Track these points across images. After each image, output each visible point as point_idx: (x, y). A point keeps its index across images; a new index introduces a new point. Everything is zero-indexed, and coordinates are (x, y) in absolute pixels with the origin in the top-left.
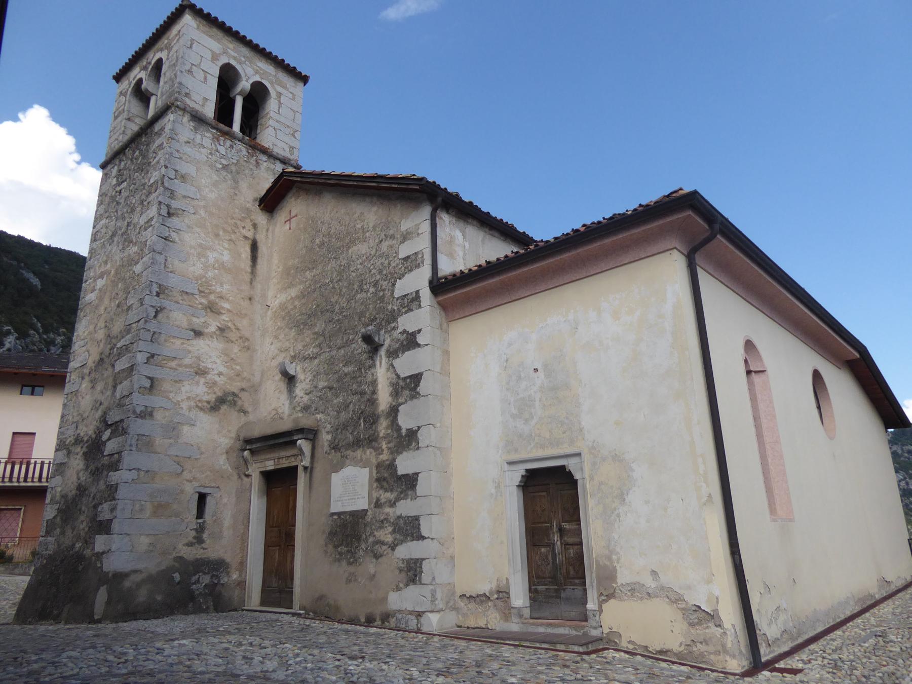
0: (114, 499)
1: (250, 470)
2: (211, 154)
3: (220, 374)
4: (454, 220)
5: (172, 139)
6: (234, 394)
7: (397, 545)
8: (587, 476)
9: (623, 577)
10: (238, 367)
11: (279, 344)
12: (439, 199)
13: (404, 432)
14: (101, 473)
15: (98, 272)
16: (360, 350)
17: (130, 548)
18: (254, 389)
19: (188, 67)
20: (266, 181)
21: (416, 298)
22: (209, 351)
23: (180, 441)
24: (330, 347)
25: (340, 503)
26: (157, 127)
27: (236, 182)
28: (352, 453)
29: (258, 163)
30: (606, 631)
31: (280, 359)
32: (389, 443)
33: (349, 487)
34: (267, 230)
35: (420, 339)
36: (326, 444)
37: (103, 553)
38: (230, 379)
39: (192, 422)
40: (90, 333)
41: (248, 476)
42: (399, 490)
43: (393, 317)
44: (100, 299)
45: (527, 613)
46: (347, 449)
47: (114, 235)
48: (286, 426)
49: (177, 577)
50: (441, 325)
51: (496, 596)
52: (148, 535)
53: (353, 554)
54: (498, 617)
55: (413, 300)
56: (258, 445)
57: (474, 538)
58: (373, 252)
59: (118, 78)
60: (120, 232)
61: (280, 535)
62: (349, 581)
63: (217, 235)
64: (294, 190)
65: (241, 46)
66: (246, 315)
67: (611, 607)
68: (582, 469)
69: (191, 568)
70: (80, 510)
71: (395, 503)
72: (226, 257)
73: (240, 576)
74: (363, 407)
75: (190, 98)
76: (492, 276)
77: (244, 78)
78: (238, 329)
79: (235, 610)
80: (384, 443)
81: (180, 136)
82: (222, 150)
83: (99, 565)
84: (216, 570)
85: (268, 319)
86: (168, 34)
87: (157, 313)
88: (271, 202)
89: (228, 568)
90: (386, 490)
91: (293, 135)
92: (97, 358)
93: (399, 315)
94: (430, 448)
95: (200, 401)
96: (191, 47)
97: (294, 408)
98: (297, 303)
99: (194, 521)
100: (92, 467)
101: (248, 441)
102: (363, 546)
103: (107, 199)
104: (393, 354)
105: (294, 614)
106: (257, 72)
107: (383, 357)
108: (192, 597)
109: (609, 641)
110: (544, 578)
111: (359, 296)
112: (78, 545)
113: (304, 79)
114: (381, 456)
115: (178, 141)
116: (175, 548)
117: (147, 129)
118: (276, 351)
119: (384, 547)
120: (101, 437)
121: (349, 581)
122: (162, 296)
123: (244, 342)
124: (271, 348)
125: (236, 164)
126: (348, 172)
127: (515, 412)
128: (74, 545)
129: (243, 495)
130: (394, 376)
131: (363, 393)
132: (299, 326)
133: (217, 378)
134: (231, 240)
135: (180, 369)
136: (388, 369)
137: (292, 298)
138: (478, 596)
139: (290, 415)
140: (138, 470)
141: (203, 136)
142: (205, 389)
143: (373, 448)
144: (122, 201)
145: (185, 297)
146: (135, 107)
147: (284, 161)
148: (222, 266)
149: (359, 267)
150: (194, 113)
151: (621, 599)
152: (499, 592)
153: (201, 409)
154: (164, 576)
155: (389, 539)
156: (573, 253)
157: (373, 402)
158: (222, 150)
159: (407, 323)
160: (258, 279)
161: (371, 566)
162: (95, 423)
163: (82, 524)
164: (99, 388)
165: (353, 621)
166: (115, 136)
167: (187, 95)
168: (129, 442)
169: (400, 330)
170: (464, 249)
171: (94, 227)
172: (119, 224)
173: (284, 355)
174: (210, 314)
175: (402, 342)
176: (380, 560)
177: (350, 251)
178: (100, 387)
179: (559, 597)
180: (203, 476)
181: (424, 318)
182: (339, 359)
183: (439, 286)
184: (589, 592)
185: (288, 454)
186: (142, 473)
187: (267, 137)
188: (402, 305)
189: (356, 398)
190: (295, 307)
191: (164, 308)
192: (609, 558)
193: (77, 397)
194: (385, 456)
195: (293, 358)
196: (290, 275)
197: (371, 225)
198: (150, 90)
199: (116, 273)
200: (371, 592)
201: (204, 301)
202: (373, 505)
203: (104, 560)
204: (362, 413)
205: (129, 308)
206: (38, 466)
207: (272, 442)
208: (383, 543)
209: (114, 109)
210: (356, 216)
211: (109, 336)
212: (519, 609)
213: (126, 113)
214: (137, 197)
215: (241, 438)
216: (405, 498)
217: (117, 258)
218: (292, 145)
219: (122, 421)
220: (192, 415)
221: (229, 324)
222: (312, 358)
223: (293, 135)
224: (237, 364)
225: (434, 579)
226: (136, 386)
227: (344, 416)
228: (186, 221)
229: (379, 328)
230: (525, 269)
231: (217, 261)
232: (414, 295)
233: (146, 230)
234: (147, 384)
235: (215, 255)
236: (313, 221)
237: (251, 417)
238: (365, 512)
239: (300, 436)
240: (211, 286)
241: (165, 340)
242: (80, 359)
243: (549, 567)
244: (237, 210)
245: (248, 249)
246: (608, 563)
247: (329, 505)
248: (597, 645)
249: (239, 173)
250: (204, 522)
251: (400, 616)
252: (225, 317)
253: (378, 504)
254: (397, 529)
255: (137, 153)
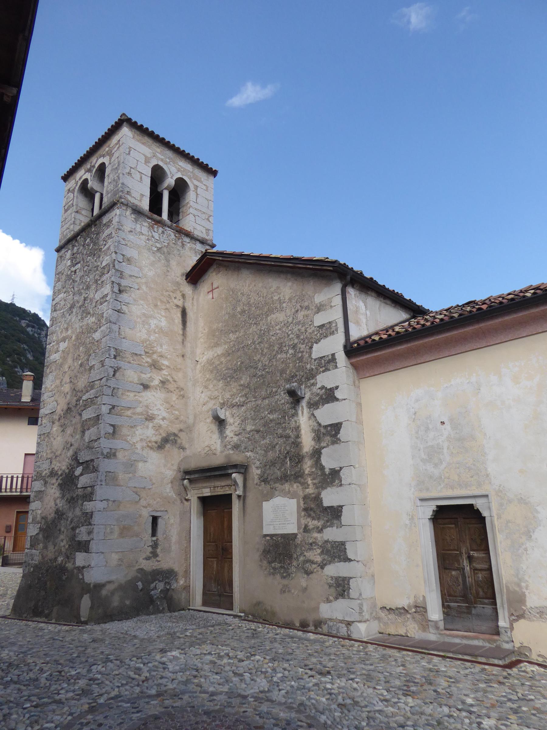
0: (90, 524)
1: (189, 496)
2: (148, 239)
3: (164, 419)
4: (357, 293)
5: (119, 229)
6: (175, 435)
7: (325, 565)
8: (494, 513)
9: (532, 601)
10: (177, 412)
11: (209, 393)
12: (348, 278)
13: (327, 471)
14: (77, 502)
15: (61, 337)
16: (283, 401)
17: (104, 564)
18: (189, 429)
19: (127, 170)
20: (192, 260)
21: (333, 359)
22: (154, 400)
23: (137, 475)
24: (255, 397)
25: (272, 527)
26: (105, 220)
27: (168, 261)
28: (280, 486)
29: (183, 245)
30: (517, 645)
31: (211, 405)
32: (314, 479)
33: (280, 514)
34: (193, 299)
35: (338, 394)
36: (256, 477)
37: (84, 567)
38: (171, 422)
39: (145, 459)
40: (57, 387)
41: (187, 500)
42: (325, 519)
43: (312, 375)
44: (64, 359)
45: (441, 625)
46: (275, 483)
47: (72, 307)
48: (218, 460)
49: (140, 585)
50: (354, 382)
51: (414, 610)
52: (117, 552)
53: (286, 570)
54: (417, 628)
55: (329, 362)
56: (196, 476)
57: (394, 564)
58: (290, 320)
59: (66, 178)
60: (78, 305)
61: (218, 549)
62: (283, 591)
63: (156, 306)
64: (215, 266)
65: (166, 149)
66: (180, 369)
67: (521, 626)
68: (489, 508)
69: (150, 577)
70: (60, 530)
71: (322, 530)
72: (164, 323)
73: (185, 581)
74: (288, 448)
75: (131, 195)
76: (401, 343)
77: (169, 176)
78: (175, 381)
79: (183, 609)
80: (309, 479)
81: (125, 227)
82: (156, 236)
83: (81, 577)
84: (167, 578)
85: (198, 371)
86: (109, 143)
87: (115, 372)
88: (195, 276)
89: (176, 576)
90: (313, 519)
91: (208, 220)
92: (65, 407)
93: (318, 373)
94: (353, 486)
95: (150, 441)
96: (129, 154)
97: (225, 446)
98: (223, 359)
99: (150, 539)
100: (68, 496)
101: (187, 472)
102: (295, 563)
103: (64, 277)
104: (313, 405)
105: (235, 616)
106: (179, 170)
107: (305, 407)
108: (152, 601)
109: (520, 654)
110: (456, 596)
111: (279, 356)
112: (60, 559)
113: (214, 173)
114: (307, 490)
115: (124, 231)
116: (137, 562)
117: (95, 222)
118: (207, 399)
119: (314, 566)
120: (74, 472)
121: (283, 591)
122: (118, 358)
123: (180, 391)
124: (203, 396)
125: (167, 247)
126: (265, 253)
127: (424, 456)
128: (56, 559)
129: (185, 516)
130: (315, 424)
131: (288, 437)
132: (226, 379)
133: (161, 422)
134: (166, 309)
135: (135, 417)
136: (310, 418)
137: (218, 356)
138: (397, 609)
139: (222, 452)
140: (107, 500)
141: (142, 225)
142: (153, 432)
143: (300, 483)
144: (78, 279)
145: (135, 358)
146: (82, 202)
147: (203, 242)
148: (161, 331)
149: (278, 331)
150: (134, 208)
151: (530, 619)
152: (416, 607)
153: (151, 448)
154: (131, 584)
155: (319, 559)
156: (476, 327)
157: (297, 444)
158: (156, 236)
159: (325, 380)
160: (188, 339)
161: (303, 581)
162: (67, 460)
163: (63, 542)
164: (69, 432)
165: (289, 625)
166: (67, 226)
167: (128, 193)
168: (100, 478)
169: (319, 386)
170: (370, 318)
171: (53, 300)
172: (76, 298)
173: (213, 402)
174: (154, 370)
175: (322, 396)
176: (310, 576)
177: (269, 318)
178: (69, 431)
179: (470, 613)
180: (155, 502)
181: (340, 376)
182: (263, 408)
183: (353, 350)
184: (500, 611)
185: (223, 484)
186: (111, 503)
187: (188, 222)
188: (320, 365)
189: (281, 441)
190: (222, 363)
191: (120, 368)
192: (519, 585)
193: (50, 439)
194: (311, 490)
195: (223, 405)
196: (214, 337)
197: (287, 297)
198: (95, 188)
199: (77, 338)
200: (304, 602)
201: (149, 360)
202: (302, 530)
203: (85, 574)
204: (288, 453)
205: (91, 368)
206: (9, 480)
207: (208, 474)
208: (312, 562)
209: (64, 204)
210: (272, 289)
211: (74, 389)
212: (436, 622)
213: (75, 207)
214: (92, 277)
215: (182, 470)
216: (331, 526)
217: (77, 326)
218: (207, 227)
219: (92, 460)
220: (144, 453)
221: (169, 378)
222: (240, 406)
223: (208, 220)
224: (175, 410)
225: (361, 594)
226: (103, 433)
227: (271, 455)
228: (133, 295)
229: (300, 383)
230: (432, 339)
231: (157, 327)
232: (330, 357)
233: (101, 304)
234: (111, 430)
235: (155, 321)
236: (233, 292)
237: (188, 452)
238: (295, 535)
239: (234, 471)
240: (154, 347)
241: (122, 394)
242: (50, 407)
243: (460, 588)
244: (170, 284)
245: (179, 315)
246: (517, 589)
247: (262, 528)
248: (514, 660)
249: (169, 254)
250: (157, 539)
251: (331, 624)
252: (165, 372)
253: (306, 530)
254: (325, 551)
255: (88, 240)
